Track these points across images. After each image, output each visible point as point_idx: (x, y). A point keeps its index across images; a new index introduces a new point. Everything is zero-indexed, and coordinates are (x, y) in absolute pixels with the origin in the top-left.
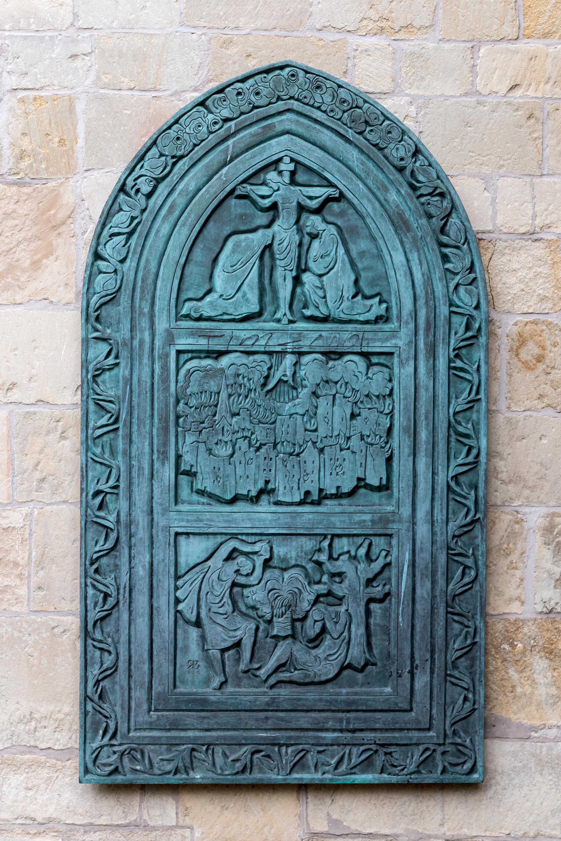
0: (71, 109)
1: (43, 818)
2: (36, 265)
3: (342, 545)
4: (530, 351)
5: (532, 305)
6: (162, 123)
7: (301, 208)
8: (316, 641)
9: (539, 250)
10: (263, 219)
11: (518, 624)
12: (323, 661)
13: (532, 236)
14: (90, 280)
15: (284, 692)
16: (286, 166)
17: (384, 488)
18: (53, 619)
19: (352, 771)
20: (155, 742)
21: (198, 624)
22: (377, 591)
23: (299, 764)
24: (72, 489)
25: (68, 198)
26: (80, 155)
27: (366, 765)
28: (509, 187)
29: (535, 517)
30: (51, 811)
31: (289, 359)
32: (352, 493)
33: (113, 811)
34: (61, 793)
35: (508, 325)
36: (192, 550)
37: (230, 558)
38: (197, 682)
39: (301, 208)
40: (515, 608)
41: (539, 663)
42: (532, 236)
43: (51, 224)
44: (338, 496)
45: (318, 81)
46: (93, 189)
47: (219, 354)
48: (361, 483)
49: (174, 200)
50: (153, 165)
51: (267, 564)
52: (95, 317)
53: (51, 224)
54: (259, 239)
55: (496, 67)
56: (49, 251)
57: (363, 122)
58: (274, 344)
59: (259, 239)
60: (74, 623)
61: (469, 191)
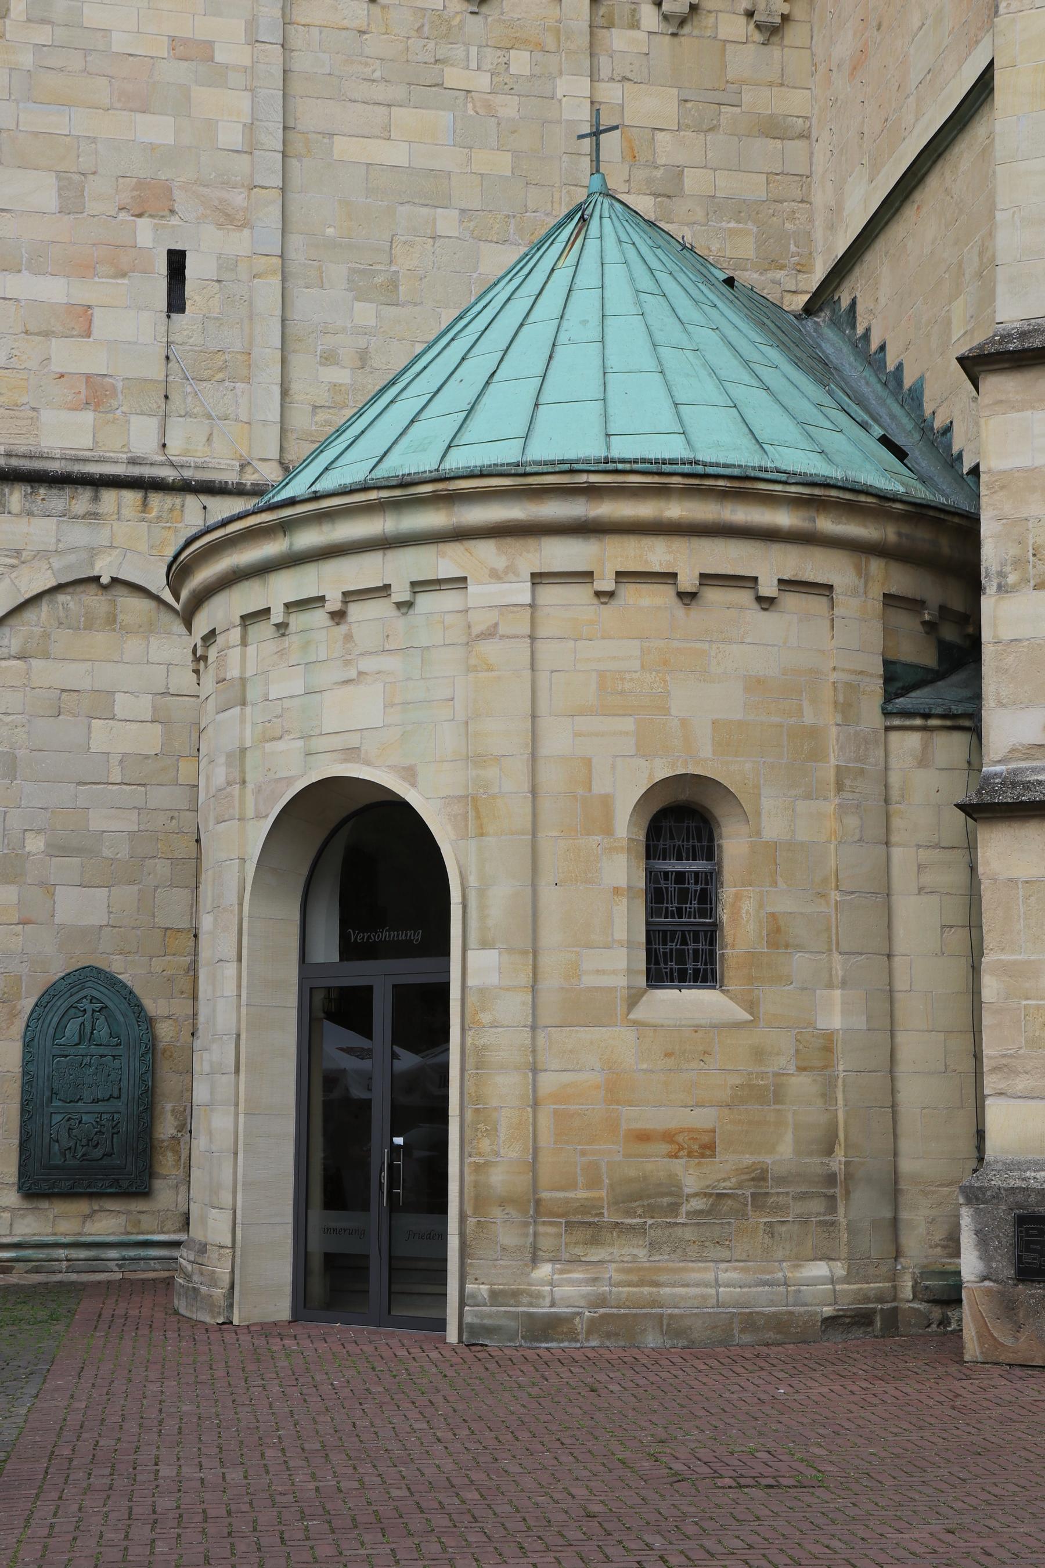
0: (21, 979)
1: (638, 868)
2: (8, 1028)
3: (104, 1116)
4: (168, 1053)
5: (168, 1039)
6: (49, 985)
7: (94, 1011)
8: (96, 1146)
9: (171, 1022)
10: (81, 1014)
11: (163, 1141)
12: (98, 1153)
13: (168, 1017)
14: (25, 1033)
15: (85, 1163)
16: (89, 998)
17: (119, 1097)
18: (10, 1141)
19: (106, 1188)
20: (43, 1179)
21: (57, 1141)
22: (115, 1130)
23: (89, 1186)
24: (17, 1099)
25: (19, 1007)
26: (23, 994)
27: (111, 1186)
28: (162, 1002)
29: (169, 1107)
30: (7, 1204)
31: (88, 1058)
32: (108, 1100)
33: (625, 826)
34: (12, 1198)
35: (161, 1046)
36: (57, 1118)
37: (68, 1120)
38: (58, 1161)
39: (94, 1011)
40: (162, 1136)
41: (169, 1154)
42: (168, 1017)
43: (13, 1015)
44: (103, 1100)
45: (99, 971)
46: (27, 1004)
47: (67, 1056)
48: (111, 1096)
49: (174, 1232)
50: (47, 998)
51: (80, 1122)
52: (27, 1045)
53: (13, 1015)
54: (80, 1020)
55: (157, 964)
56: (12, 1024)
57: (112, 982)
58: (84, 1053)
59: (80, 1020)
60: (17, 1142)
61: (148, 1004)
